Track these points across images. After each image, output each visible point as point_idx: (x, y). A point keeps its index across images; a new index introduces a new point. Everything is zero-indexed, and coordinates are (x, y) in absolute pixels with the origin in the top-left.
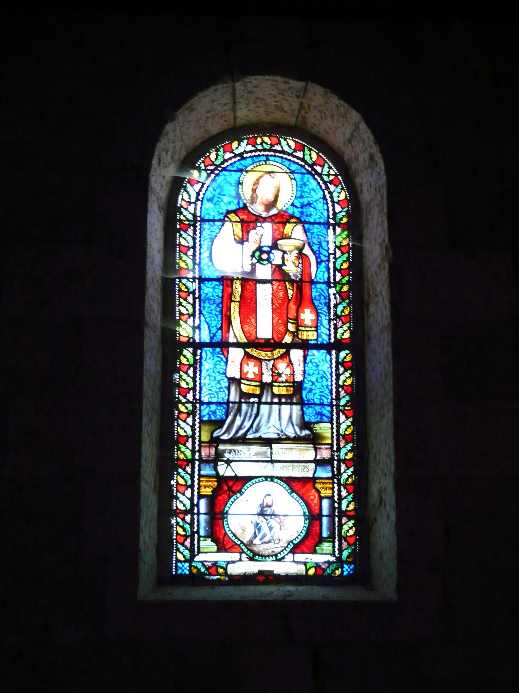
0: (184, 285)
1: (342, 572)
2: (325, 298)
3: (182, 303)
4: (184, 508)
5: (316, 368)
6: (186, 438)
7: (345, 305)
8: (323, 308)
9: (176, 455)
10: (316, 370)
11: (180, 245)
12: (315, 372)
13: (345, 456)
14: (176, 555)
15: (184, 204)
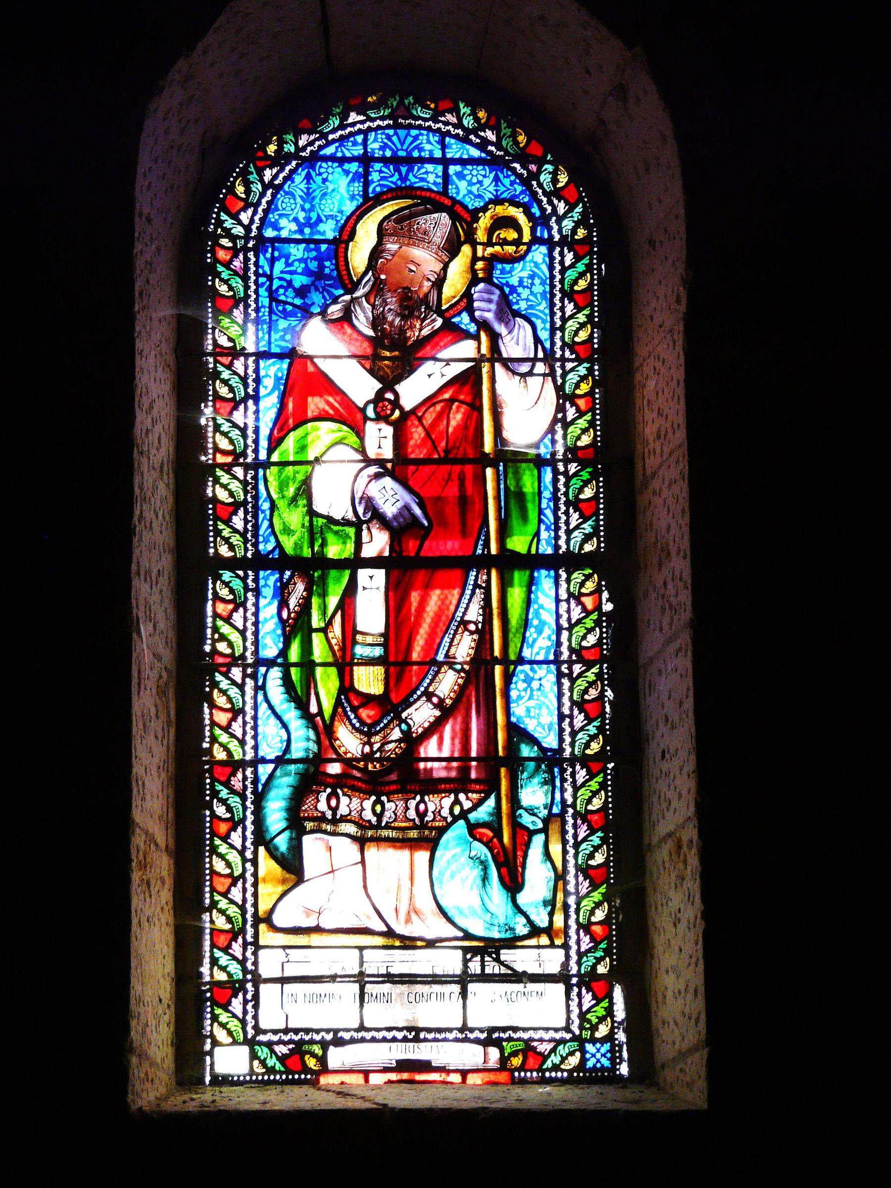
0: (227, 584)
1: (583, 1060)
2: (543, 283)
3: (220, 426)
4: (231, 500)
5: (525, 685)
6: (231, 509)
7: (599, 954)
8: (540, 304)
9: (212, 551)
10: (525, 690)
11: (215, 500)
12: (523, 694)
13: (587, 805)
14: (211, 862)
15: (222, 718)
